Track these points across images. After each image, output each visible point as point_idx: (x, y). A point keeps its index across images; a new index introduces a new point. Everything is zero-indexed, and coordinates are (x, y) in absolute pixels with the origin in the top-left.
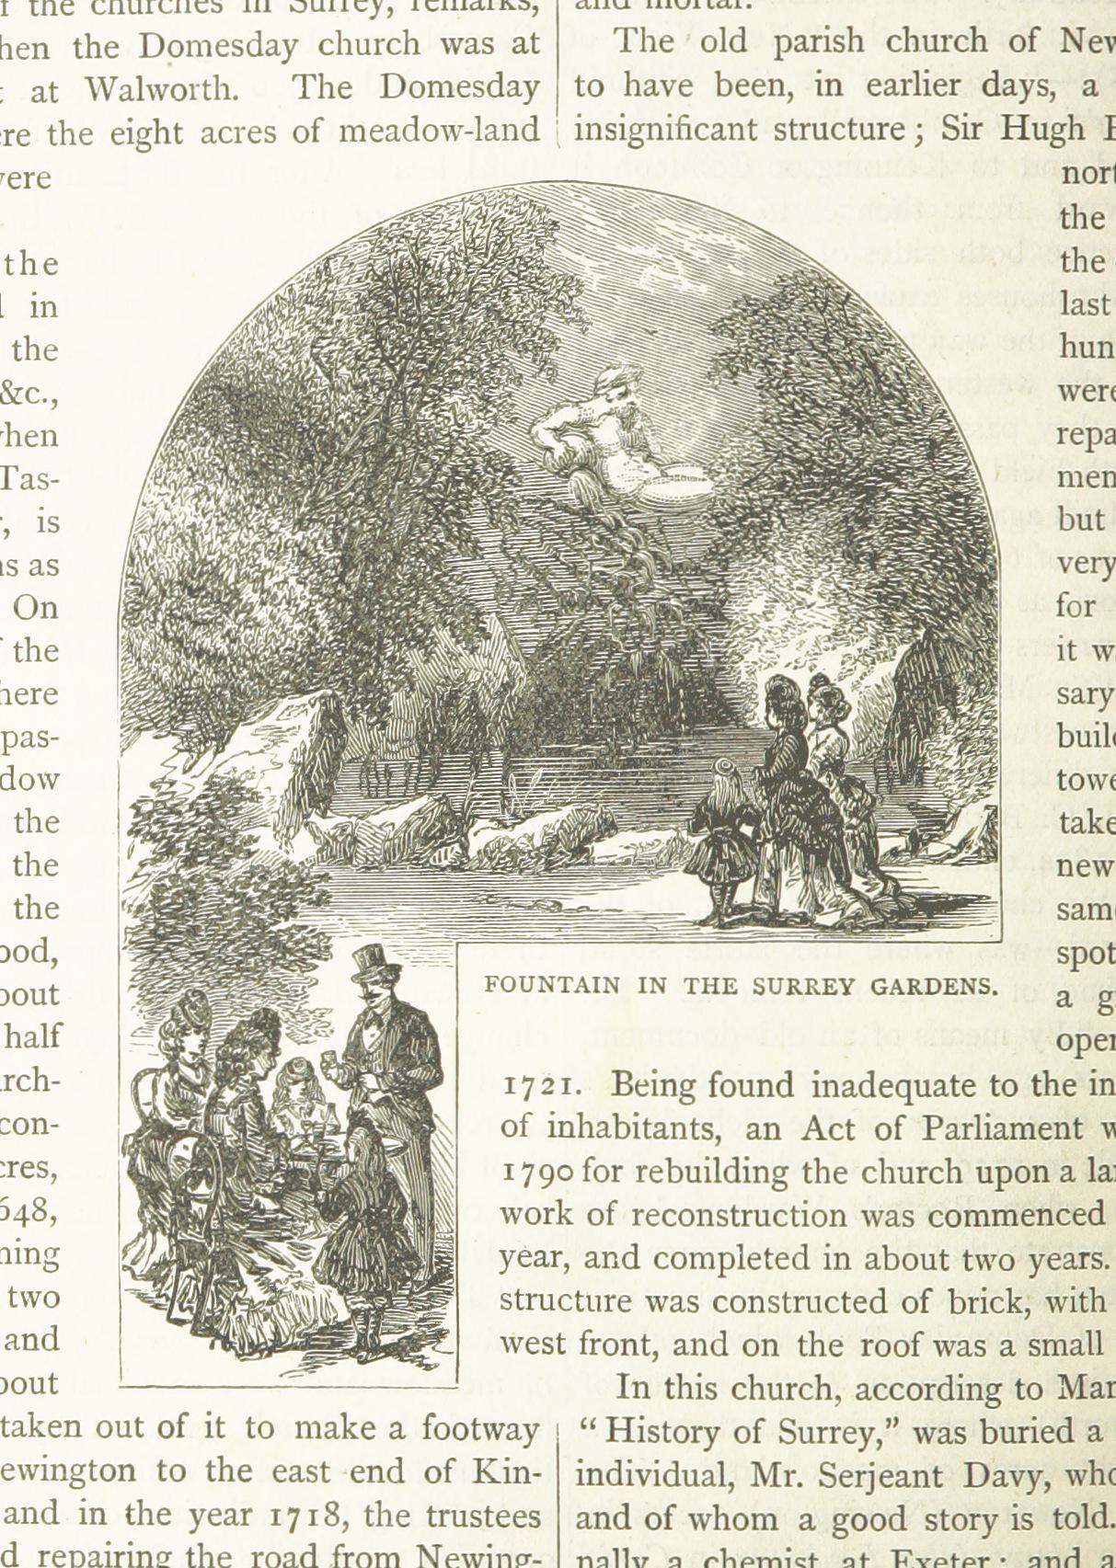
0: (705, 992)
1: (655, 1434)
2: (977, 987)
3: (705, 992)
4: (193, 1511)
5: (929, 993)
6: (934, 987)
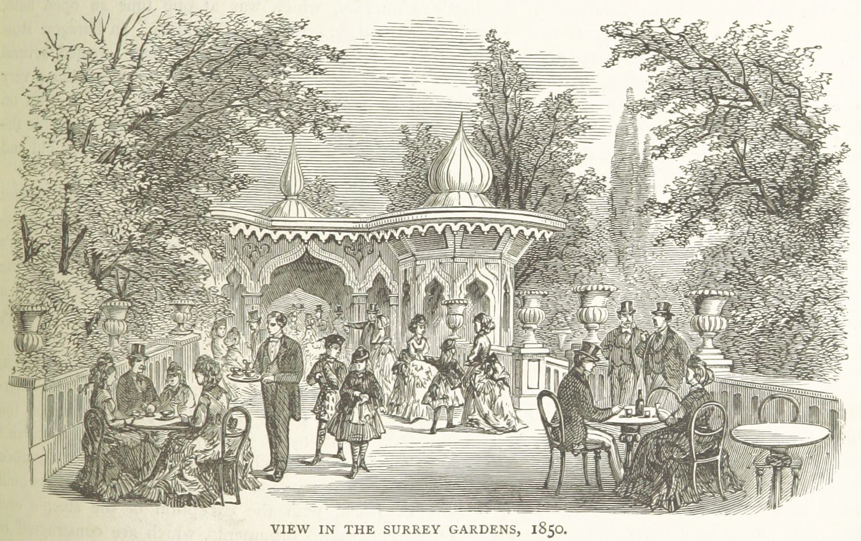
0: (357, 533)
1: (98, 469)
2: (509, 530)
3: (357, 533)
4: (273, 526)
5: (481, 532)
6: (484, 529)
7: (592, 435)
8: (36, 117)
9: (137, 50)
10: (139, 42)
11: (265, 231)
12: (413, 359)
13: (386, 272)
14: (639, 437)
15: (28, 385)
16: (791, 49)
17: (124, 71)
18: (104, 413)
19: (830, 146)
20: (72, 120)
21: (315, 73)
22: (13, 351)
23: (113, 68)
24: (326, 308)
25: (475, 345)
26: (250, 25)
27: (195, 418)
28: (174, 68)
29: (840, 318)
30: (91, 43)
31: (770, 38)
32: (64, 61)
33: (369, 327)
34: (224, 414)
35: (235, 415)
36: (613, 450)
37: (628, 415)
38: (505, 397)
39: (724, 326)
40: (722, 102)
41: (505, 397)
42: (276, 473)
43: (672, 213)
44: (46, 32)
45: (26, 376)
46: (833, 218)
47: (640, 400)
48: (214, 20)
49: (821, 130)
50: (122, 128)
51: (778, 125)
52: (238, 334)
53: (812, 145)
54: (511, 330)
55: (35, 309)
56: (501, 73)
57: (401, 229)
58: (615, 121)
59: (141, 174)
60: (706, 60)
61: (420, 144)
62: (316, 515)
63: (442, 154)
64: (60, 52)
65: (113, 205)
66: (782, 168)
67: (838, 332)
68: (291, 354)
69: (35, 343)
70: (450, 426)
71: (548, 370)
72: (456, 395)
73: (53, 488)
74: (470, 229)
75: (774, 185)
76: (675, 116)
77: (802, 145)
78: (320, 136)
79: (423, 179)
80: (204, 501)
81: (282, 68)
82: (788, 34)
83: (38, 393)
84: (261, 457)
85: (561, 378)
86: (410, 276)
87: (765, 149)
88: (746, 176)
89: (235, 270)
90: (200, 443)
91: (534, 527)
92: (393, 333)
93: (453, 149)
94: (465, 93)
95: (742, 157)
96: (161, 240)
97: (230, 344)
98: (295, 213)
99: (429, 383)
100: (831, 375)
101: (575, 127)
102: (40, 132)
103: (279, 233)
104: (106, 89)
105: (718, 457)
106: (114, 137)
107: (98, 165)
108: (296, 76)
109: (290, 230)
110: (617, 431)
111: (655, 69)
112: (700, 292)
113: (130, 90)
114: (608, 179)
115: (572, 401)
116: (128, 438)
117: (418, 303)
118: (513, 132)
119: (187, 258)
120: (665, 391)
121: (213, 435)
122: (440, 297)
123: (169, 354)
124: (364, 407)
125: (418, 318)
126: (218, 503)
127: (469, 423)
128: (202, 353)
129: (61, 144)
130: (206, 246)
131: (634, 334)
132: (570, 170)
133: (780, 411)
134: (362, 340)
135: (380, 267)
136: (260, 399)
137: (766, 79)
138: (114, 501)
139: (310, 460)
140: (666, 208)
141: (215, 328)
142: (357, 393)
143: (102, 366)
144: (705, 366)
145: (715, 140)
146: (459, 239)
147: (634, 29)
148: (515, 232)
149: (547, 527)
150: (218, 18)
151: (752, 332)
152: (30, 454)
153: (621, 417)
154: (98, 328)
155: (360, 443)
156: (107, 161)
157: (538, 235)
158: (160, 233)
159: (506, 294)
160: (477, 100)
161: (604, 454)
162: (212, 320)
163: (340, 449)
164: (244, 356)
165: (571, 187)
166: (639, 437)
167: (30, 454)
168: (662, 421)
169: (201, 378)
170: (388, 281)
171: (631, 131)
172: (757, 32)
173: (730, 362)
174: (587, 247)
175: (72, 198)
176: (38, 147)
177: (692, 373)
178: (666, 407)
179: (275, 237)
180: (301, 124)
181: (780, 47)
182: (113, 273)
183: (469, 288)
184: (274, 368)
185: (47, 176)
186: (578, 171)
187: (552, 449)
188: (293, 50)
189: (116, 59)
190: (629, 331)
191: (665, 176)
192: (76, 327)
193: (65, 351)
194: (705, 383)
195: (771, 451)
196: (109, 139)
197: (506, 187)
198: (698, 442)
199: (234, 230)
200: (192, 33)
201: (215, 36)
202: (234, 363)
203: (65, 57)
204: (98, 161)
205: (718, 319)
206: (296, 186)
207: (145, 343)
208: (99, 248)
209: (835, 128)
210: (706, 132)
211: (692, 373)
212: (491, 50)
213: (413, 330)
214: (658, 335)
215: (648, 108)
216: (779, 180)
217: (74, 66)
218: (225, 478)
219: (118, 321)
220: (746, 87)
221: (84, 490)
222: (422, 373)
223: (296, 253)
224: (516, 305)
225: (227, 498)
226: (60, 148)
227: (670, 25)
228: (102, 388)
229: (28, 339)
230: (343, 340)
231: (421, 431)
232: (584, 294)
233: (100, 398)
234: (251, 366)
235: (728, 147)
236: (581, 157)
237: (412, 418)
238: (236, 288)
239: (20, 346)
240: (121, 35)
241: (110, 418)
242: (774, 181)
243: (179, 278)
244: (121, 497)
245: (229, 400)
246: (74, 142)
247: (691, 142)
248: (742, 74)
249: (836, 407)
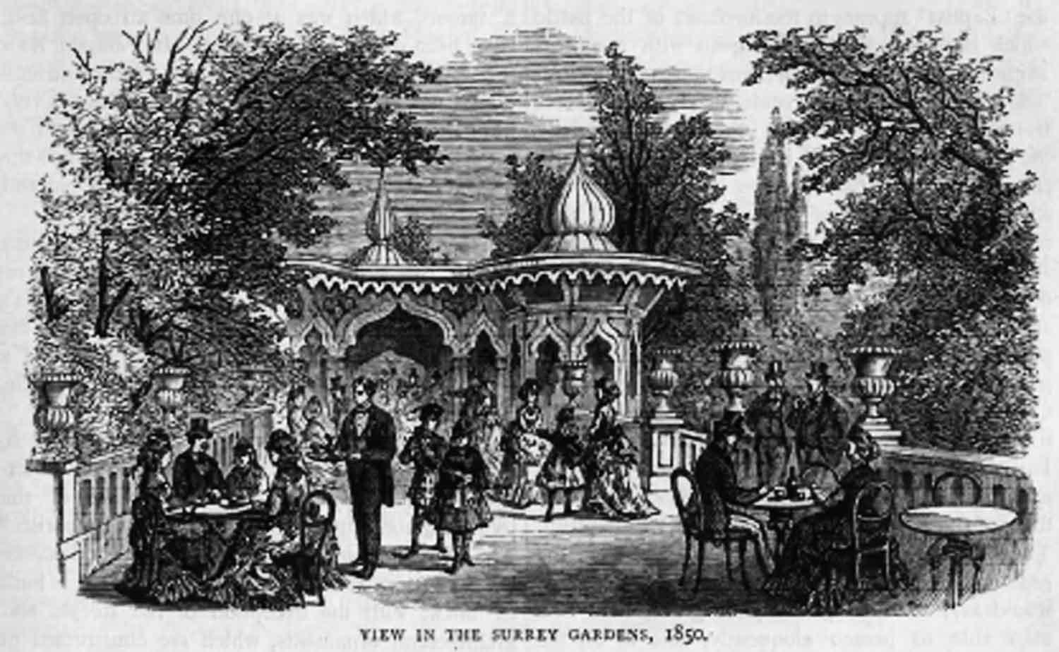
2: (639, 636)
7: (736, 522)
8: (61, 150)
9: (194, 70)
10: (196, 61)
11: (350, 282)
12: (524, 431)
13: (492, 331)
14: (791, 524)
15: (56, 469)
16: (964, 60)
17: (175, 96)
18: (159, 502)
19: (1014, 174)
20: (111, 153)
21: (407, 96)
22: (32, 430)
23: (164, 91)
24: (421, 371)
25: (597, 416)
26: (328, 40)
27: (269, 504)
28: (239, 91)
29: (1028, 379)
30: (136, 64)
31: (939, 47)
32: (99, 84)
33: (473, 396)
34: (303, 499)
35: (316, 500)
36: (760, 538)
37: (778, 498)
38: (633, 478)
39: (892, 389)
40: (884, 124)
41: (633, 478)
42: (365, 569)
43: (827, 256)
44: (74, 50)
45: (50, 457)
46: (1018, 261)
47: (792, 477)
48: (287, 34)
49: (1002, 156)
50: (176, 163)
51: (949, 151)
52: (319, 404)
53: (992, 175)
54: (638, 398)
55: (62, 378)
56: (623, 92)
57: (508, 279)
58: (759, 148)
59: (200, 217)
60: (864, 74)
61: (529, 178)
62: (413, 617)
63: (557, 186)
64: (94, 74)
65: (165, 254)
66: (956, 202)
67: (1027, 396)
68: (382, 427)
69: (64, 419)
70: (568, 513)
71: (683, 445)
72: (577, 474)
73: (90, 589)
74: (590, 277)
75: (946, 221)
76: (829, 142)
77: (979, 173)
78: (413, 170)
79: (536, 221)
80: (280, 603)
81: (368, 90)
82: (962, 43)
83: (68, 479)
84: (348, 549)
85: (698, 453)
86: (520, 333)
87: (944, 183)
88: (914, 211)
89: (314, 330)
90: (276, 534)
91: (669, 631)
92: (500, 400)
93: (569, 181)
94: (581, 116)
95: (909, 188)
96: (225, 294)
97: (309, 416)
98: (386, 261)
99: (543, 460)
100: (1018, 446)
101: (717, 156)
102: (67, 169)
103: (366, 285)
104: (155, 117)
105: (886, 547)
106: (165, 174)
107: (146, 207)
108: (383, 99)
109: (379, 280)
110: (765, 518)
111: (804, 87)
112: (862, 350)
113: (185, 118)
114: (752, 215)
115: (713, 482)
116: (183, 529)
117: (529, 369)
118: (639, 161)
119: (257, 315)
120: (821, 469)
121: (290, 523)
122: (555, 359)
123: (237, 428)
124: (467, 490)
125: (529, 383)
126: (297, 605)
127: (590, 511)
128: (276, 427)
129: (96, 181)
130: (281, 302)
131: (783, 402)
132: (707, 206)
133: (958, 489)
134: (463, 413)
135: (483, 324)
136: (344, 481)
137: (935, 96)
138: (170, 605)
139: (405, 552)
140: (820, 250)
141: (292, 396)
142: (459, 473)
143: (154, 445)
144: (869, 437)
145: (877, 168)
146: (576, 291)
147: (780, 39)
148: (642, 280)
149: (684, 632)
150: (294, 34)
151: (925, 396)
152: (60, 550)
153: (770, 499)
154: (147, 400)
155: (462, 534)
156: (157, 202)
157: (670, 284)
158: (224, 287)
159: (633, 355)
160: (597, 124)
161: (750, 547)
162: (288, 389)
163: (440, 539)
164: (327, 429)
165: (708, 226)
166: (791, 524)
167: (60, 550)
168: (818, 503)
169: (276, 457)
170: (493, 340)
171: (777, 159)
172: (925, 40)
173: (898, 433)
174: (730, 296)
175: (112, 246)
176: (63, 186)
177: (853, 446)
178: (825, 486)
179: (361, 290)
180: (391, 156)
181: (953, 58)
182: (167, 334)
183: (589, 346)
184: (362, 445)
185: (76, 220)
186: (717, 207)
187: (688, 539)
188: (382, 68)
189: (166, 82)
190: (779, 396)
191: (819, 211)
192: (119, 399)
193: (103, 427)
194: (871, 457)
195: (949, 540)
196: (160, 175)
197: (632, 227)
198: (860, 530)
199: (313, 282)
200: (260, 51)
201: (289, 53)
202: (315, 439)
203: (100, 81)
204: (145, 203)
205: (884, 383)
206: (385, 229)
207: (208, 417)
208: (148, 304)
209: (1018, 153)
210: (865, 160)
211: (853, 446)
212: (613, 66)
213: (524, 397)
214: (813, 401)
215: (798, 132)
216: (953, 216)
217: (113, 88)
218: (304, 577)
219: (174, 391)
220: (911, 105)
221: (134, 590)
222: (536, 448)
223: (389, 308)
224: (644, 367)
225: (308, 598)
226: (95, 186)
227: (822, 33)
228: (155, 470)
229: (54, 414)
230: (441, 411)
231: (532, 518)
232: (726, 355)
233: (152, 484)
234: (334, 442)
235: (892, 177)
236: (719, 192)
237: (524, 502)
238: (314, 348)
239: (40, 422)
240: (173, 56)
241: (165, 506)
242: (947, 216)
243: (251, 342)
244: (181, 599)
245: (309, 482)
246: (113, 179)
247: (849, 171)
248: (907, 91)
249: (1023, 484)
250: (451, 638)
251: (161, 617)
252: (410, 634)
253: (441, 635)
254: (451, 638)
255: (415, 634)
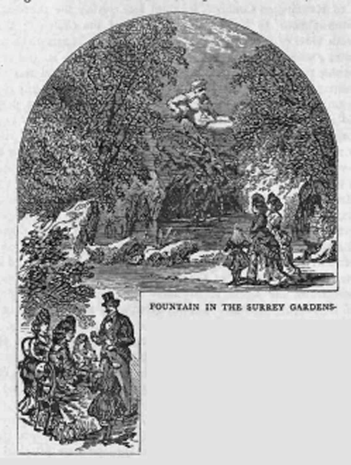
250: (225, 309)
251: (342, 150)
252: (202, 307)
253: (219, 308)
254: (225, 309)
255: (205, 307)
